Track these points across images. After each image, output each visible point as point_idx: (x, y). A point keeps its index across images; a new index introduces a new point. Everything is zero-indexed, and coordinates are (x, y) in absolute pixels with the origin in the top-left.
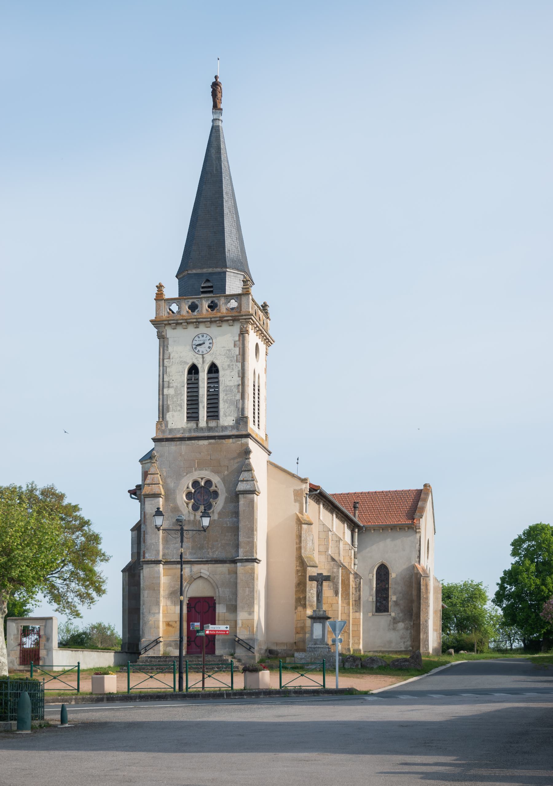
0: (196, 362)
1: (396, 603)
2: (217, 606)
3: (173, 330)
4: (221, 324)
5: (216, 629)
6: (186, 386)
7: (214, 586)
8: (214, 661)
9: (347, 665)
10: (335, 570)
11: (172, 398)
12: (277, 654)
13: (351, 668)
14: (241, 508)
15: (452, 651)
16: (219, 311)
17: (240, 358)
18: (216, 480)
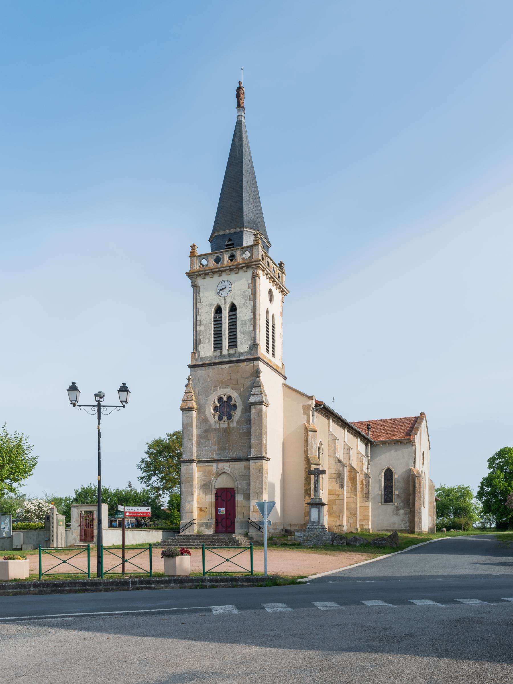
0: (220, 304)
1: (398, 496)
2: (236, 494)
3: (203, 280)
4: (237, 271)
5: (136, 511)
6: (213, 323)
7: (234, 479)
8: (224, 539)
9: (335, 543)
10: (341, 469)
11: (203, 333)
12: (291, 533)
13: (338, 546)
14: (253, 416)
15: (445, 529)
16: (236, 261)
17: (252, 297)
18: (235, 395)
